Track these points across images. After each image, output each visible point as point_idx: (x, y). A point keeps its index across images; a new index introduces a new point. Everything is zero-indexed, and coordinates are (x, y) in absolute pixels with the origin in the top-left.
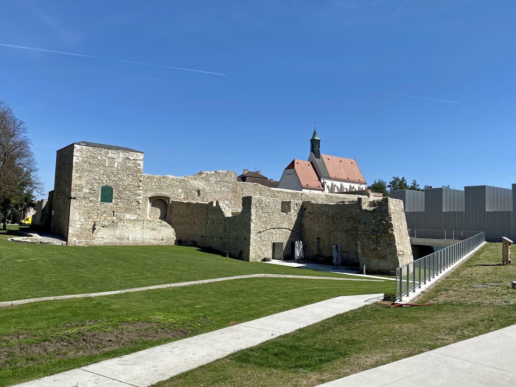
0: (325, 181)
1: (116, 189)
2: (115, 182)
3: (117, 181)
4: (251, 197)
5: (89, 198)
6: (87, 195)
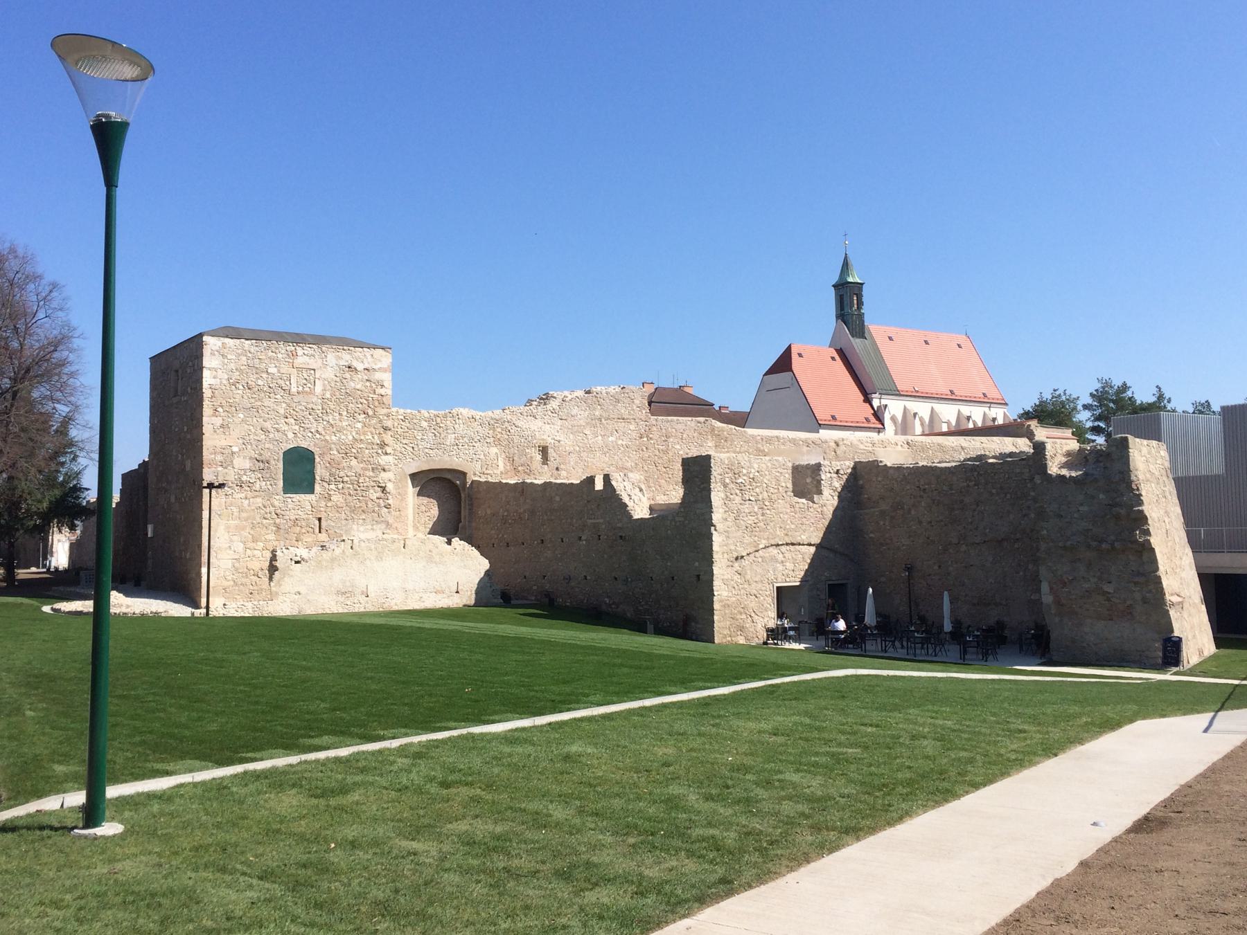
0: (884, 402)
1: (321, 455)
2: (318, 436)
3: (323, 433)
4: (708, 457)
5: (250, 485)
6: (245, 477)
